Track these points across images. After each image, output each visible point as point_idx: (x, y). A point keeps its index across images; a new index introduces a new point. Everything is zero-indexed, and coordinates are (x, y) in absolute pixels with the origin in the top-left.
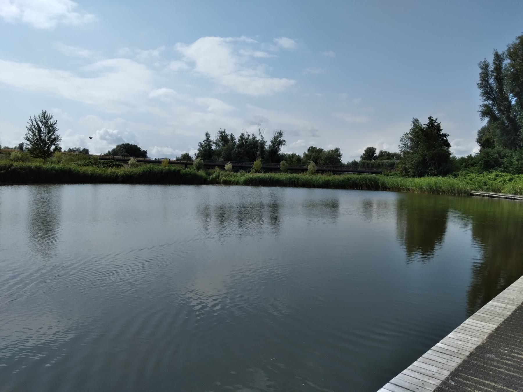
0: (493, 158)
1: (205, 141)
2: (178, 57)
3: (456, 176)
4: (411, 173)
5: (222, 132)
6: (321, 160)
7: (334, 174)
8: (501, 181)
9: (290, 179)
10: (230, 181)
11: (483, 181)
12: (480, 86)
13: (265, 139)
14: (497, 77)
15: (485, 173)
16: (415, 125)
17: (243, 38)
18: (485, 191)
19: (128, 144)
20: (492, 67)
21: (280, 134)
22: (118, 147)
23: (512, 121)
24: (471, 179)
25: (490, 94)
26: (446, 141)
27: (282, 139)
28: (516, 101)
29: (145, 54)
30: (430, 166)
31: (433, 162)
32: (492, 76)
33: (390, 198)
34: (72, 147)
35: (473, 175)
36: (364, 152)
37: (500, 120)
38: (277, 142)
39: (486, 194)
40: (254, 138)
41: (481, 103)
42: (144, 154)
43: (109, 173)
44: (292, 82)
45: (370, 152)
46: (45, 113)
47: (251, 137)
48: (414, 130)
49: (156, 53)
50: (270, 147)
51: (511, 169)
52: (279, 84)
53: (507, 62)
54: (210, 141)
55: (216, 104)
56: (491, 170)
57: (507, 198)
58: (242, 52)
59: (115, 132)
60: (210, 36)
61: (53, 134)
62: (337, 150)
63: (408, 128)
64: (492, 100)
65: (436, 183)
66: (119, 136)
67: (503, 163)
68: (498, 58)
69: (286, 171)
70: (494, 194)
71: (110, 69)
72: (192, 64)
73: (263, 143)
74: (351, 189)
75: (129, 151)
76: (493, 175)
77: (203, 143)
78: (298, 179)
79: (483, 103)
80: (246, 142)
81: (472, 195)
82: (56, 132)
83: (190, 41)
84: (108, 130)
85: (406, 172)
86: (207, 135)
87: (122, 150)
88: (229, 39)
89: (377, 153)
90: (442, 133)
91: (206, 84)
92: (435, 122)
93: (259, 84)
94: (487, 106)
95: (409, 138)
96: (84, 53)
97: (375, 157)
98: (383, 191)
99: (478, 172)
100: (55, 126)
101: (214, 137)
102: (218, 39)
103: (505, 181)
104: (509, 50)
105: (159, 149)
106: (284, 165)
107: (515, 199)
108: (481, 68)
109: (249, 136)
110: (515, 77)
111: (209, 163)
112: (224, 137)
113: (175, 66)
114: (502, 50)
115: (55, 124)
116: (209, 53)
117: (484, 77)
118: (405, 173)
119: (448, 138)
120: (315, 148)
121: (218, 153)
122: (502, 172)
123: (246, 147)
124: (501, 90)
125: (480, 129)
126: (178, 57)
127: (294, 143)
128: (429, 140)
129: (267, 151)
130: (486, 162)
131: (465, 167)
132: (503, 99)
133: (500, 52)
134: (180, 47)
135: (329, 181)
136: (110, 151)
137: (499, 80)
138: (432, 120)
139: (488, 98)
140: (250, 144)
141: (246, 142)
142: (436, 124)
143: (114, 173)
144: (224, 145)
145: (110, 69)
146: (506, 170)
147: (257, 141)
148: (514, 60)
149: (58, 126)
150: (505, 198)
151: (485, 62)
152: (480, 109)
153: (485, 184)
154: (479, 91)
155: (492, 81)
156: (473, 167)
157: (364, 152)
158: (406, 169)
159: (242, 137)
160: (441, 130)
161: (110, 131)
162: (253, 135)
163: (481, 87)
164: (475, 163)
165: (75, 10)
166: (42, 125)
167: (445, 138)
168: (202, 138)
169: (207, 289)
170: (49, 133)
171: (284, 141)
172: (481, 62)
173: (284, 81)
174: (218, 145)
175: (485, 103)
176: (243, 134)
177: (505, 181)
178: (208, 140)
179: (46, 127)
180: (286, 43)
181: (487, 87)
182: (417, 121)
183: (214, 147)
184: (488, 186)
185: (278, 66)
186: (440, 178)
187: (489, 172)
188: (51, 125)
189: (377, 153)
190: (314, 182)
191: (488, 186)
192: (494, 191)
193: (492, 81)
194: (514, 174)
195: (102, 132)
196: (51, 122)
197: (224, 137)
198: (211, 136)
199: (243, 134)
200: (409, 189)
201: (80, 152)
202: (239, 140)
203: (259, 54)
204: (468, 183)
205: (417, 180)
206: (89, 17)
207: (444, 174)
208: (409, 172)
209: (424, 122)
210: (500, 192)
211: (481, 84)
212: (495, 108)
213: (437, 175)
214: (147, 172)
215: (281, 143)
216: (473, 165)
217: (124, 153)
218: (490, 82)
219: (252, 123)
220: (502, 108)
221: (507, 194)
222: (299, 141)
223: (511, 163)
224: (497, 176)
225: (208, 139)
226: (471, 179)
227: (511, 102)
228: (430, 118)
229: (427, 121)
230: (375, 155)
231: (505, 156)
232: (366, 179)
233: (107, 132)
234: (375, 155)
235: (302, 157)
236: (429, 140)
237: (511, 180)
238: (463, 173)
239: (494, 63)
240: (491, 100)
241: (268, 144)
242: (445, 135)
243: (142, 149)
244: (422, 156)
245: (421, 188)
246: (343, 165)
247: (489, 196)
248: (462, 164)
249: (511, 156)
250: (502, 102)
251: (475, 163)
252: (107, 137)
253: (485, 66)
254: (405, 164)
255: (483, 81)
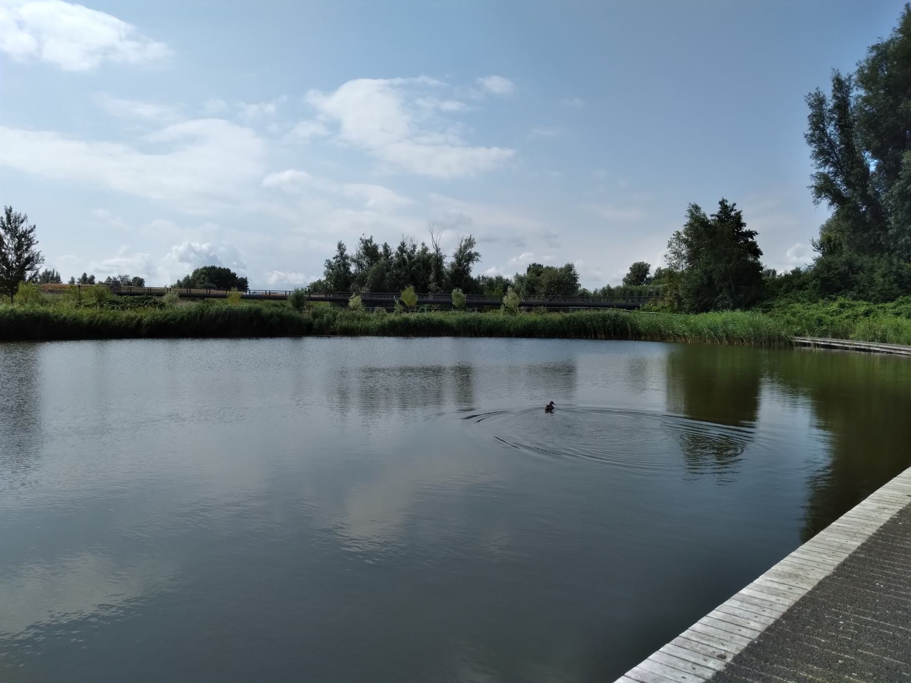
0: (839, 273)
1: (337, 257)
2: (311, 114)
3: (767, 309)
4: (687, 306)
5: (367, 241)
6: (542, 286)
7: (550, 311)
8: (848, 317)
9: (465, 321)
10: (353, 329)
11: (815, 317)
12: (811, 140)
13: (443, 252)
14: (839, 120)
15: (821, 301)
16: (692, 215)
17: (422, 79)
18: (819, 337)
19: (213, 268)
20: (830, 103)
21: (470, 243)
22: (196, 272)
23: (872, 202)
24: (794, 315)
25: (829, 154)
26: (754, 244)
27: (473, 250)
28: (878, 167)
29: (252, 110)
30: (721, 291)
31: (727, 283)
32: (832, 119)
33: (655, 354)
34: (115, 275)
35: (798, 306)
36: (629, 272)
37: (850, 202)
38: (465, 257)
39: (821, 341)
40: (425, 250)
41: (814, 171)
42: (242, 284)
43: (124, 319)
44: (510, 152)
45: (639, 271)
46: (10, 210)
47: (419, 249)
48: (690, 225)
49: (271, 108)
50: (452, 265)
51: (871, 293)
52: (488, 156)
53: (857, 93)
54: (347, 258)
55: (379, 196)
56: (834, 296)
57: (857, 349)
58: (420, 102)
59: (205, 247)
60: (363, 77)
61: (27, 250)
62: (569, 268)
63: (680, 222)
64: (834, 165)
65: (725, 323)
66: (212, 254)
67: (857, 282)
68: (840, 85)
69: (461, 308)
70: (835, 342)
71: (192, 139)
72: (335, 126)
73: (439, 259)
74: (586, 338)
75: (218, 279)
76: (835, 306)
77: (334, 261)
78: (480, 321)
79: (817, 171)
80: (410, 257)
81: (791, 345)
82: (33, 248)
83: (331, 85)
84: (193, 245)
85: (679, 304)
86: (340, 247)
87: (204, 279)
88: (398, 81)
89: (652, 273)
90: (744, 229)
91: (358, 161)
92: (732, 210)
93: (452, 159)
94: (824, 177)
95: (686, 241)
96: (147, 111)
97: (648, 279)
98: (635, 340)
99: (810, 300)
100: (31, 235)
101: (353, 250)
102: (382, 82)
103: (857, 316)
104: (860, 71)
105: (282, 274)
106: (458, 296)
107: (870, 351)
108: (811, 106)
109: (414, 246)
110: (871, 123)
111: (475, 300)
112: (369, 250)
113: (305, 130)
114: (849, 69)
115: (30, 232)
116: (364, 106)
117: (818, 121)
118: (678, 306)
119: (756, 238)
120: (540, 265)
121: (361, 280)
122: (854, 299)
123: (411, 267)
124: (849, 148)
125: (824, 223)
126: (311, 114)
127: (514, 260)
128: (720, 247)
129: (448, 273)
130: (827, 280)
131: (787, 291)
132: (852, 163)
133: (844, 76)
134: (314, 98)
135: (535, 323)
136: (181, 280)
137: (844, 126)
138: (726, 207)
139: (826, 162)
140: (418, 261)
141: (410, 257)
142: (733, 213)
143: (133, 319)
144: (371, 265)
145: (192, 139)
146: (863, 295)
147: (430, 256)
148: (871, 90)
149: (36, 235)
150: (853, 349)
151: (818, 94)
152: (813, 183)
153: (820, 322)
154: (810, 149)
155: (831, 129)
156: (801, 292)
157: (629, 272)
158: (679, 298)
159: (402, 249)
160: (744, 225)
161: (196, 245)
162: (423, 244)
163: (812, 141)
164: (805, 284)
165: (130, 37)
166: (7, 233)
167: (750, 240)
168: (332, 253)
169: (368, 520)
170: (18, 247)
171: (477, 254)
172: (810, 94)
173: (495, 151)
174: (360, 265)
175: (821, 170)
176: (403, 244)
177: (857, 316)
178: (342, 256)
179: (13, 237)
180: (497, 85)
181: (824, 141)
182: (697, 208)
183: (353, 268)
184: (825, 327)
185: (481, 126)
186: (738, 313)
187: (831, 299)
188: (25, 235)
189: (652, 273)
190: (510, 326)
191: (825, 327)
192: (835, 335)
193: (831, 129)
194: (876, 302)
195: (182, 248)
196: (23, 227)
197: (369, 250)
198: (347, 248)
199: (403, 244)
200: (678, 336)
201: (129, 284)
202: (397, 255)
203: (450, 106)
204: (788, 322)
205: (693, 318)
206: (156, 49)
207: (746, 306)
208: (684, 303)
209: (710, 211)
210: (847, 338)
211: (811, 135)
212: (839, 181)
213: (733, 309)
214: (196, 314)
215: (471, 257)
216: (800, 287)
217: (206, 284)
218: (828, 131)
219: (444, 227)
220: (852, 179)
221: (858, 340)
222: (523, 255)
223: (872, 282)
224: (842, 306)
225: (342, 254)
226: (794, 315)
227: (867, 168)
228: (722, 203)
229: (716, 209)
230: (648, 276)
231: (861, 268)
232: (605, 318)
233: (191, 249)
234: (648, 276)
235: (514, 282)
236: (720, 247)
237: (867, 314)
238: (782, 303)
239: (835, 96)
240: (831, 166)
241: (449, 260)
242: (751, 234)
243: (239, 276)
244: (705, 272)
245: (699, 333)
246: (585, 294)
247: (824, 346)
248: (781, 287)
249: (872, 270)
250: (852, 168)
251: (805, 284)
252: (192, 255)
253: (818, 102)
254: (677, 289)
255: (814, 130)
